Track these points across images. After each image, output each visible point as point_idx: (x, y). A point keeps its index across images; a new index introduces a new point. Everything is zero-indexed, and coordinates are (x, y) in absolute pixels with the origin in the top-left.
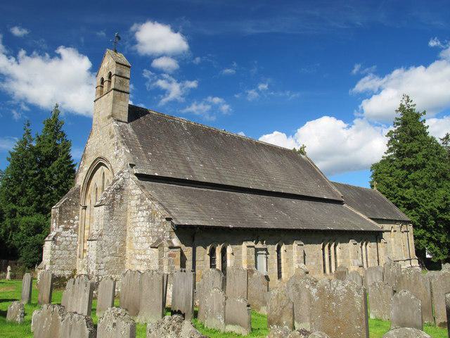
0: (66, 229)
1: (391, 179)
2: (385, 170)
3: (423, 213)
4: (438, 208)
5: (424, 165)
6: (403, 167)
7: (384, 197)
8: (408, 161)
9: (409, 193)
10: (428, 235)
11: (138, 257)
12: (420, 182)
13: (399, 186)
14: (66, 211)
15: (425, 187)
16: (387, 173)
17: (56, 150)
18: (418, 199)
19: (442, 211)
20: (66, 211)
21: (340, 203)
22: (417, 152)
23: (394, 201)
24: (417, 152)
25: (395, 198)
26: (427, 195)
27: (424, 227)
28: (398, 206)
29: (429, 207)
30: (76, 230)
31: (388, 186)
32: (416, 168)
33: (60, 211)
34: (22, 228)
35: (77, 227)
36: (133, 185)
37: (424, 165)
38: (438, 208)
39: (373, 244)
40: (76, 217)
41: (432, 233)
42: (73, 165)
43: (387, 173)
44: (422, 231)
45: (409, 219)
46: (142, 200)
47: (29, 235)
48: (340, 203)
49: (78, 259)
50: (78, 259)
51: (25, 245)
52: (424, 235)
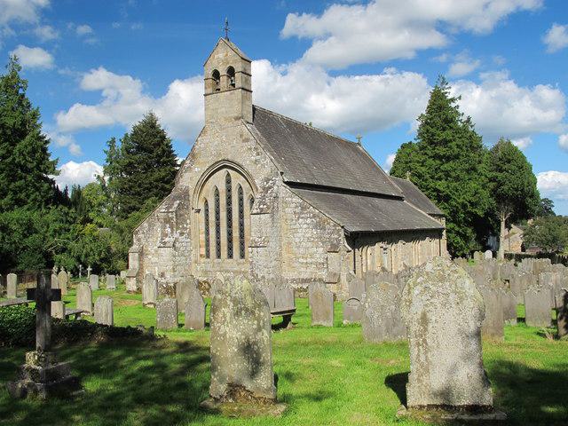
0: (182, 234)
1: (424, 169)
2: (417, 159)
3: (455, 206)
4: (469, 202)
5: (457, 157)
6: (436, 157)
7: (416, 188)
8: (441, 150)
9: (441, 185)
10: (457, 229)
11: (301, 260)
12: (453, 174)
13: (432, 177)
14: (181, 215)
15: (457, 179)
16: (418, 162)
17: (23, 124)
18: (451, 192)
19: (472, 204)
20: (181, 215)
21: (400, 199)
22: (450, 141)
23: (427, 193)
24: (450, 141)
25: (427, 189)
26: (459, 188)
27: (454, 222)
28: (430, 198)
29: (461, 201)
30: (189, 234)
31: (420, 176)
32: (448, 159)
33: (176, 215)
34: (14, 227)
35: (190, 232)
36: (285, 191)
37: (457, 157)
38: (469, 202)
39: (438, 240)
40: (188, 221)
41: (459, 226)
42: (47, 142)
43: (418, 162)
44: (452, 225)
45: (442, 213)
46: (303, 208)
47: (25, 236)
48: (400, 199)
49: (193, 265)
50: (193, 265)
51: (24, 249)
52: (453, 229)
